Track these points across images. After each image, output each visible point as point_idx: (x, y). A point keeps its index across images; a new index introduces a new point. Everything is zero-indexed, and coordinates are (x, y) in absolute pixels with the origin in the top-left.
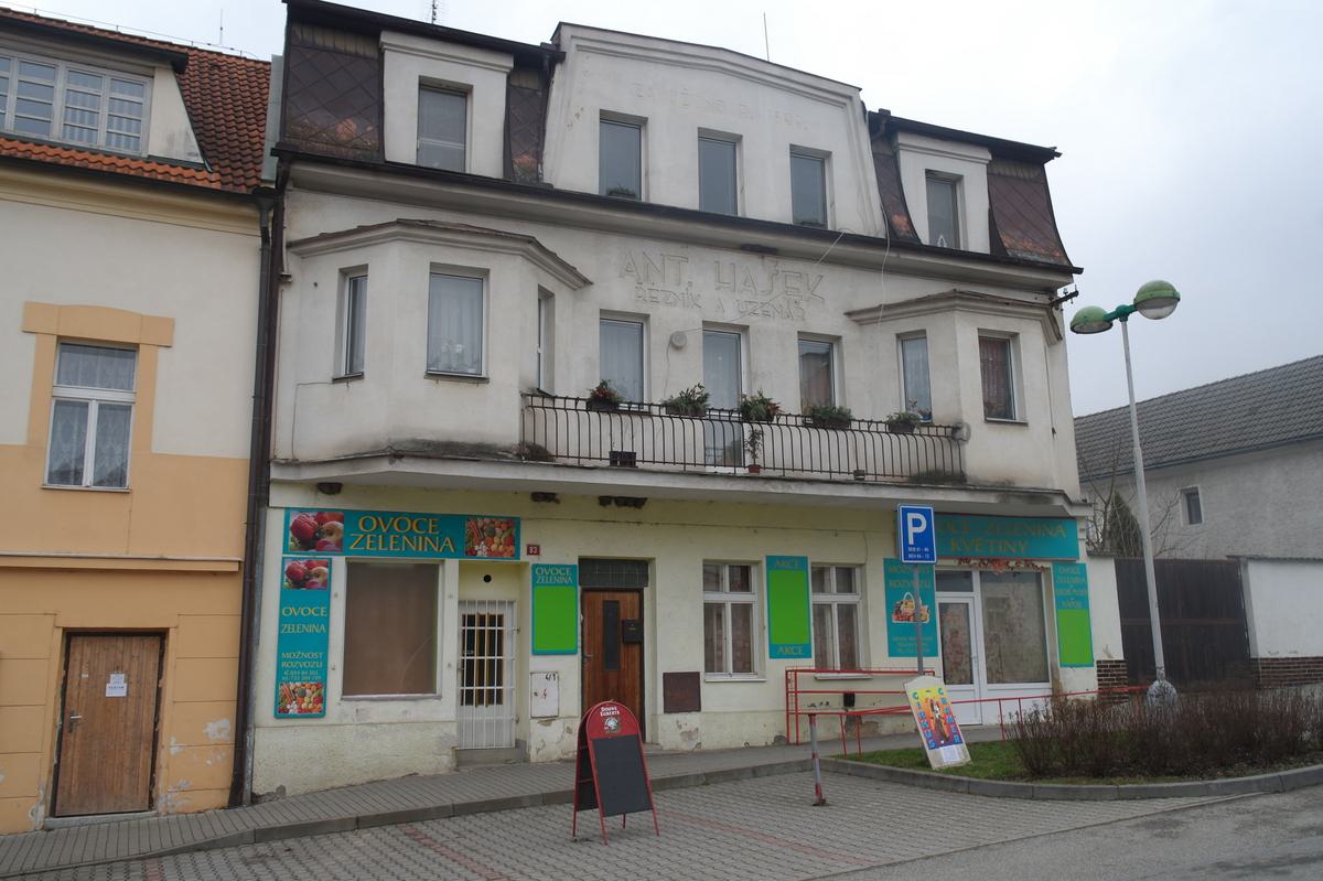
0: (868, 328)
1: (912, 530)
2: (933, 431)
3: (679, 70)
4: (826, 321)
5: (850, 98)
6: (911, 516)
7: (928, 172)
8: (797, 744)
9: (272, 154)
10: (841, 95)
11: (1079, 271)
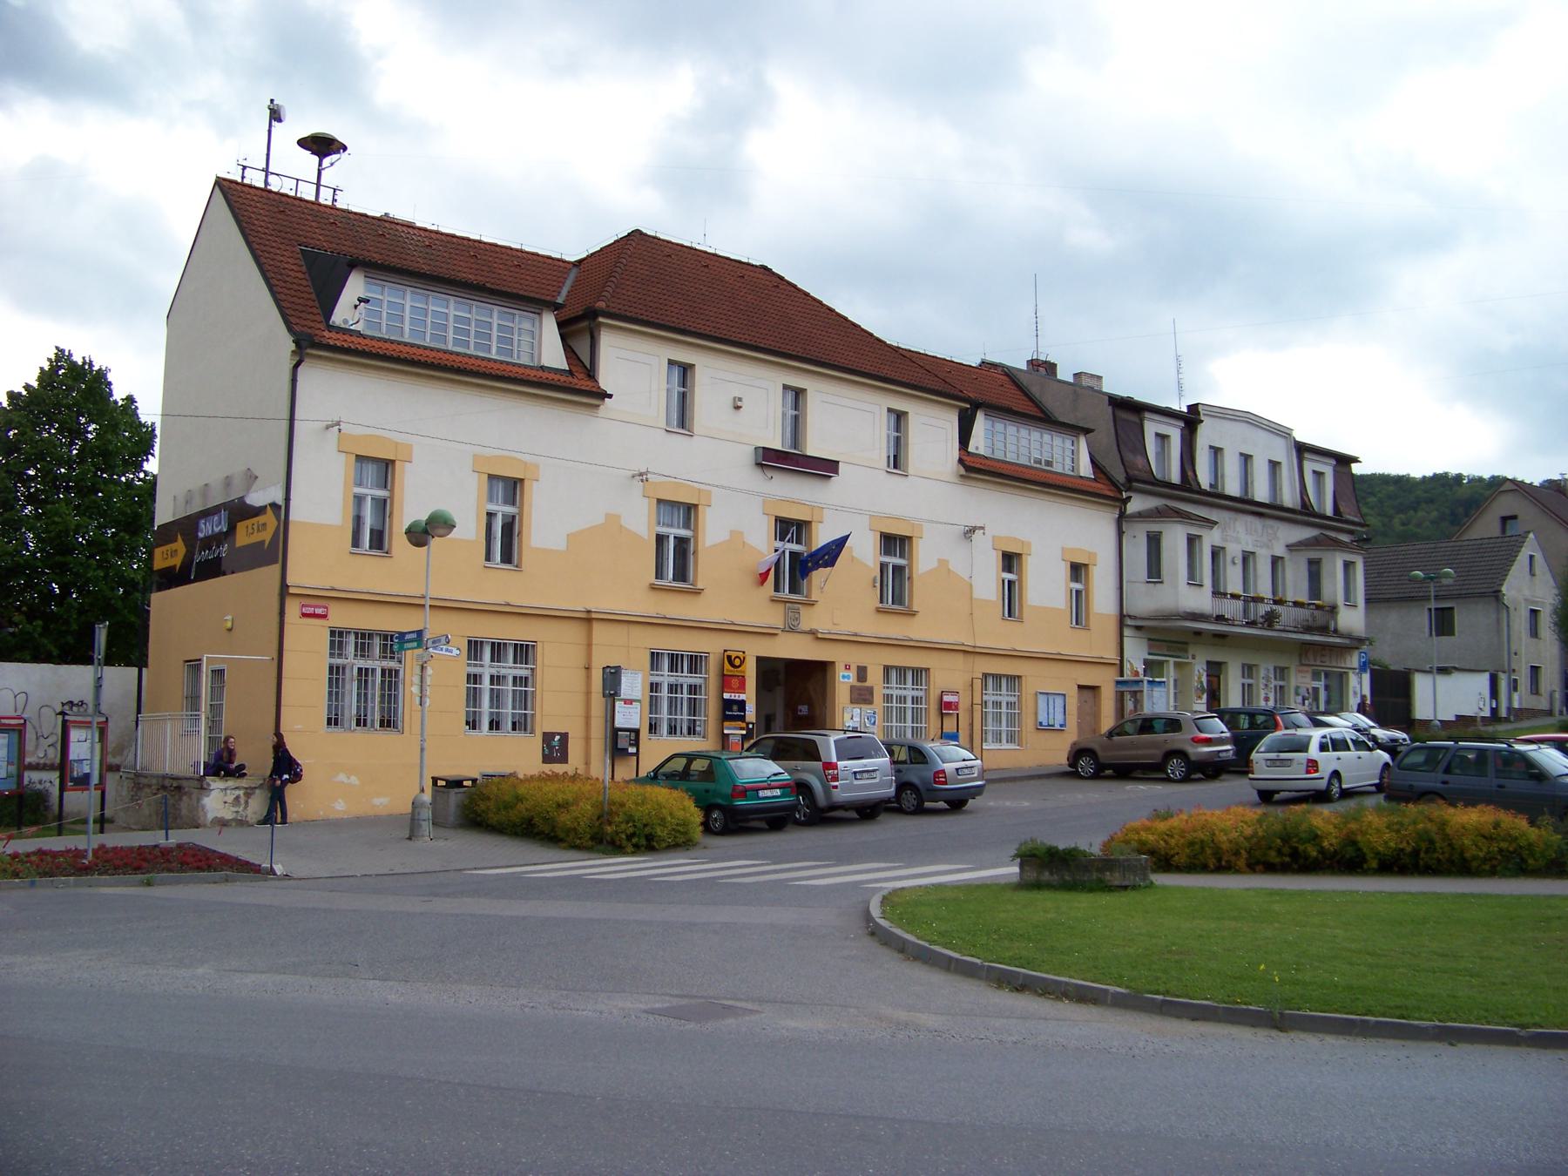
0: (1294, 553)
3: (1233, 423)
4: (1280, 551)
5: (1289, 434)
8: (902, 746)
10: (1283, 433)
11: (610, 396)
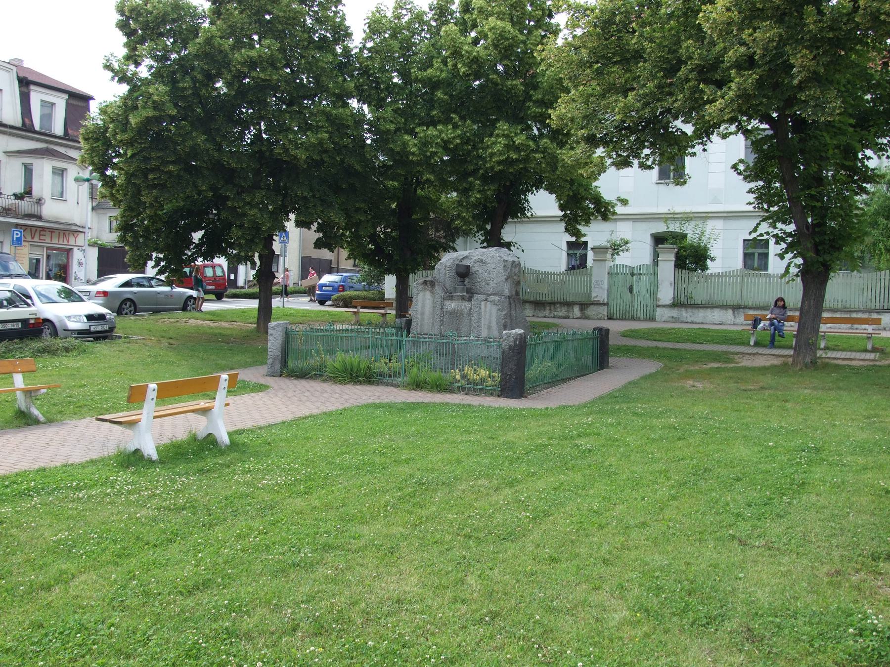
1: (15, 236)
2: (31, 200)
6: (15, 232)
7: (42, 101)
9: (680, 178)
